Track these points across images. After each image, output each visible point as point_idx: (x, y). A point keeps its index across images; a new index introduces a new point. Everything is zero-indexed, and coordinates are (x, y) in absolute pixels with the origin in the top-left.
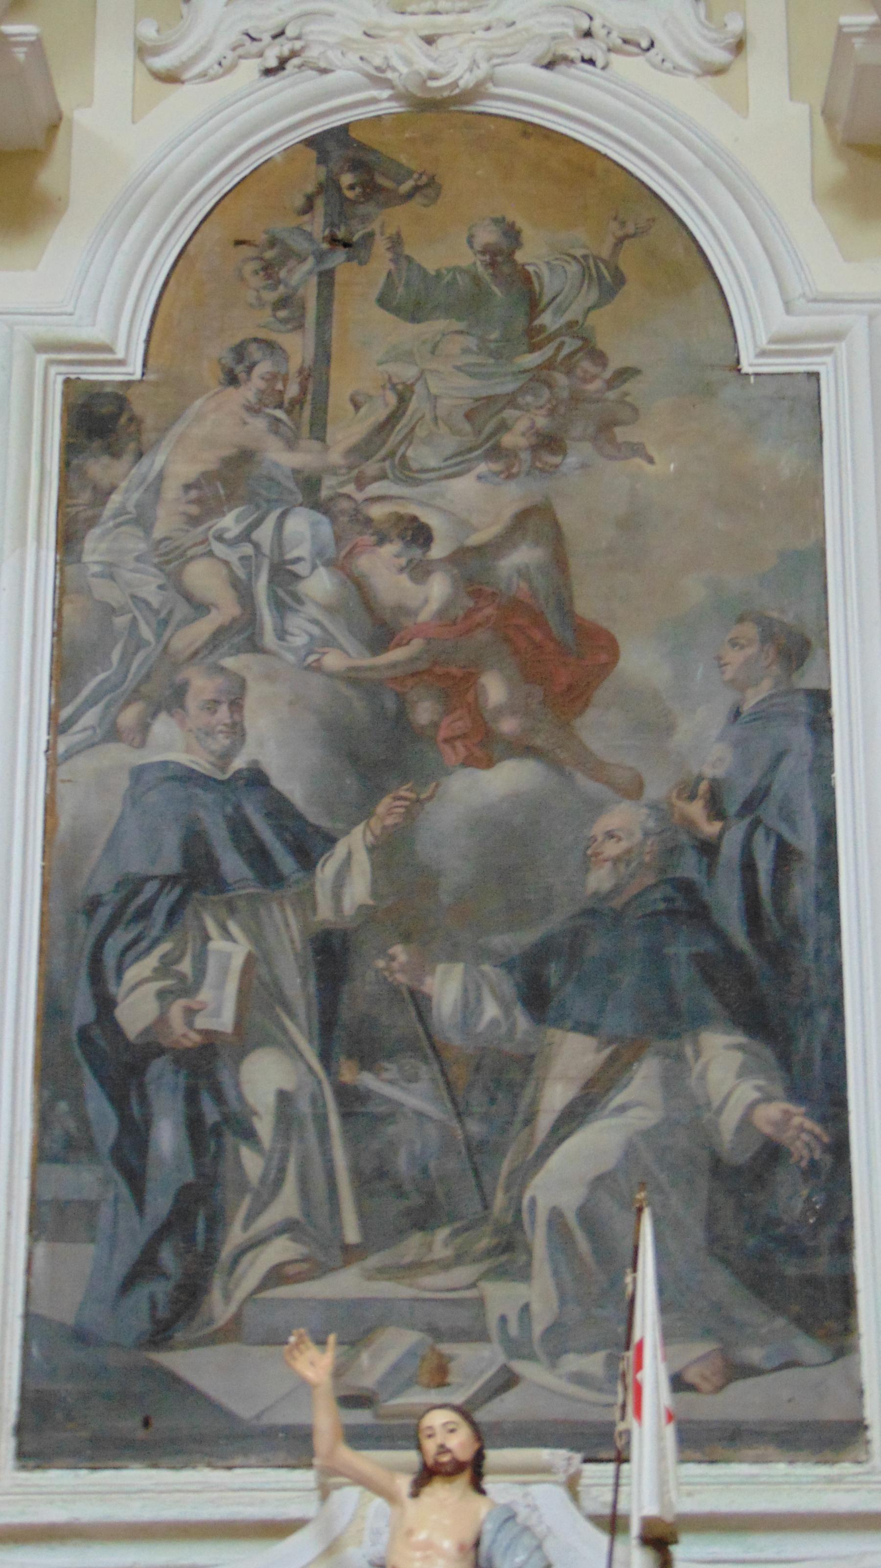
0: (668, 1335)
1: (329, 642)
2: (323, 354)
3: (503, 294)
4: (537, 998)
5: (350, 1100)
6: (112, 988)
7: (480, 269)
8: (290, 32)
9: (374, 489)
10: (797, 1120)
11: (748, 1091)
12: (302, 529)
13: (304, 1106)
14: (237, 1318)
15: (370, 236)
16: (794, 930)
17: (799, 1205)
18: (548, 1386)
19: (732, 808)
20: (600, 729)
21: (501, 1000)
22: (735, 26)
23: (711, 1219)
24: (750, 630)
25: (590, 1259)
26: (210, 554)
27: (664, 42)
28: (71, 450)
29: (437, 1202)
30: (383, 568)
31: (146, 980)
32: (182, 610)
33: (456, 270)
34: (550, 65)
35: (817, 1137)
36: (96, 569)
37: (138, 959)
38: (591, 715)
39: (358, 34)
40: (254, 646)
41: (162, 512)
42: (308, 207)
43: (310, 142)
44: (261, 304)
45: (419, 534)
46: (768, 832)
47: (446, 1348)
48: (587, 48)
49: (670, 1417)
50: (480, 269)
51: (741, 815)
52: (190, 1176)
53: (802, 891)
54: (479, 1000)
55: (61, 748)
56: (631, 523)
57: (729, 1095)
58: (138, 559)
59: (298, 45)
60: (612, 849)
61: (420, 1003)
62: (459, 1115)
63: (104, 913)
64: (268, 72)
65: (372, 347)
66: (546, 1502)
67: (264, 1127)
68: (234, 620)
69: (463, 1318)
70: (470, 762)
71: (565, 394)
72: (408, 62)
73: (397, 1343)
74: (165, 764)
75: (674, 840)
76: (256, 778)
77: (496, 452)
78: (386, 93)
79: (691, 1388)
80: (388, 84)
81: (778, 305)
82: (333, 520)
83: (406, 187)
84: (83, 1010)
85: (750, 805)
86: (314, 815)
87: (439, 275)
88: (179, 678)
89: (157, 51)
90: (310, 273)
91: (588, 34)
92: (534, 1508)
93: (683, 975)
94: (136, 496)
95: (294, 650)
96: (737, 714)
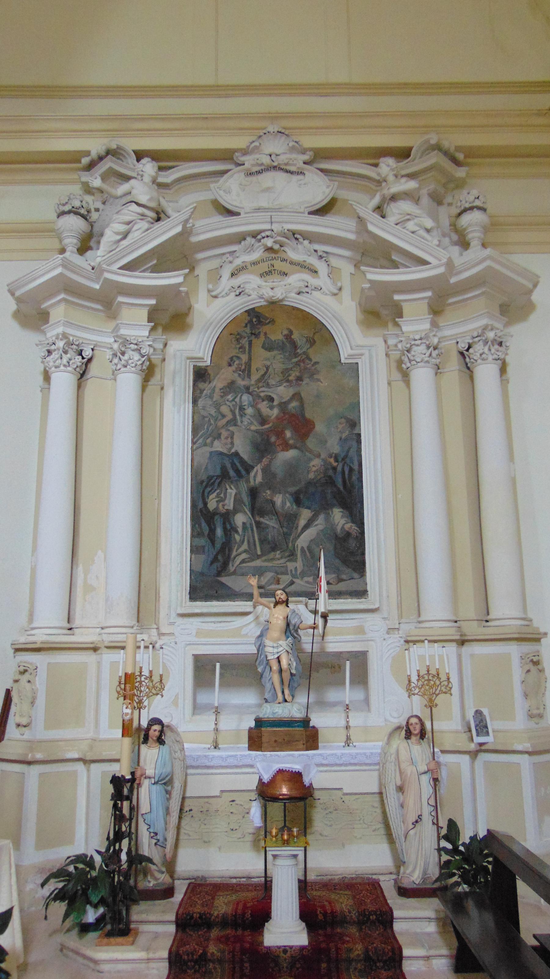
0: (326, 573)
1: (252, 423)
2: (250, 359)
3: (289, 345)
4: (298, 501)
5: (258, 524)
6: (207, 500)
7: (284, 340)
8: (242, 286)
9: (261, 389)
10: (353, 527)
11: (343, 521)
12: (246, 398)
13: (248, 525)
14: (235, 570)
15: (260, 332)
16: (353, 486)
17: (354, 545)
18: (300, 584)
19: (340, 460)
20: (311, 443)
21: (290, 503)
22: (339, 284)
23: (335, 548)
24: (343, 420)
25: (309, 557)
26: (226, 404)
27: (324, 288)
28: (195, 381)
29: (277, 545)
30: (263, 407)
31: (213, 499)
32: (220, 417)
33: (279, 340)
34: (299, 294)
35: (357, 530)
36: (201, 408)
37: (212, 493)
38: (310, 439)
39: (256, 287)
40: (235, 425)
41: (215, 395)
42: (246, 326)
43: (246, 311)
44: (236, 348)
45: (271, 399)
46: (347, 465)
47: (279, 576)
48: (307, 290)
49: (327, 592)
50: (284, 340)
51: (341, 462)
52: (224, 540)
53: (354, 478)
54: (286, 502)
55: (194, 448)
56: (318, 396)
57: (339, 523)
58: (210, 405)
59: (243, 289)
60: (314, 469)
61: (273, 503)
62: (282, 527)
63: (204, 484)
64: (236, 295)
65: (261, 357)
66: (301, 608)
67: (240, 530)
68: (231, 419)
69: (283, 570)
70: (283, 450)
71: (302, 368)
72: (268, 294)
73: (269, 575)
74: (217, 451)
75: (327, 466)
76: (237, 454)
77: (288, 381)
78: (263, 300)
79: (331, 584)
80: (263, 298)
81: (349, 348)
82: (252, 396)
83: (268, 321)
84: (201, 505)
85: (343, 459)
86: (250, 462)
87: (275, 341)
88: (219, 432)
89: (212, 291)
90: (246, 341)
91: (307, 286)
92: (299, 609)
93: (329, 496)
94: (209, 391)
95: (244, 426)
96: (341, 439)
